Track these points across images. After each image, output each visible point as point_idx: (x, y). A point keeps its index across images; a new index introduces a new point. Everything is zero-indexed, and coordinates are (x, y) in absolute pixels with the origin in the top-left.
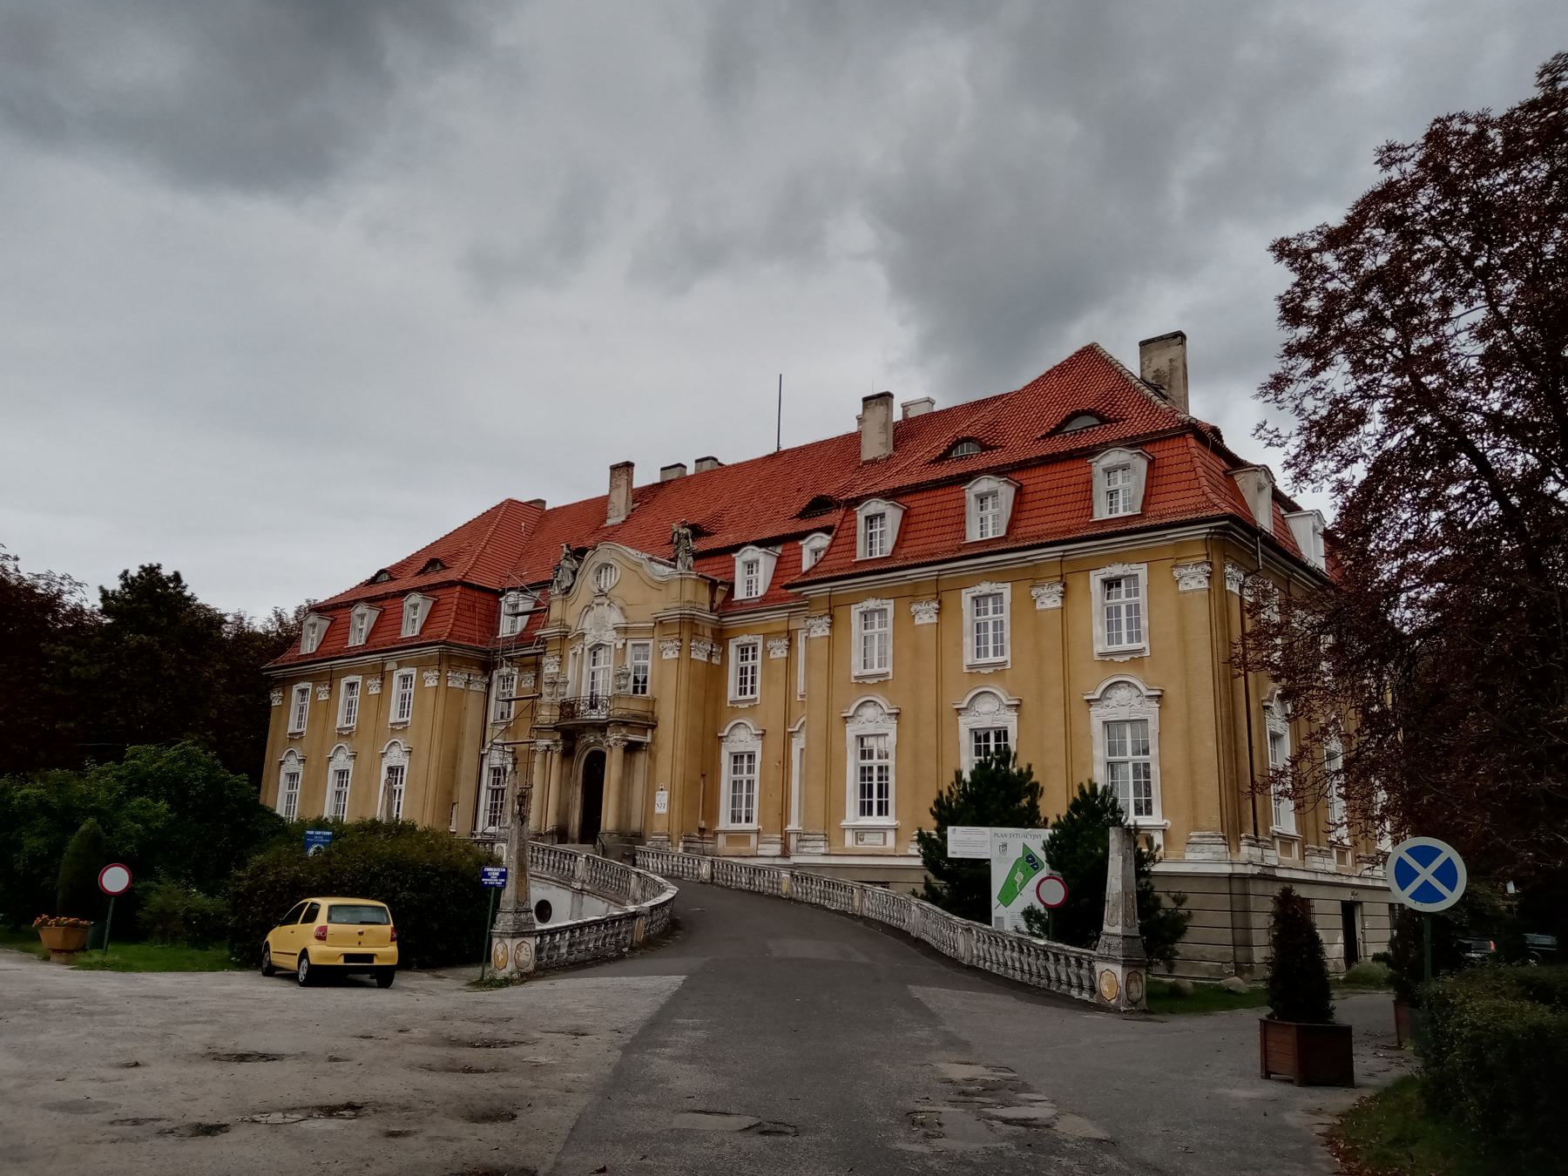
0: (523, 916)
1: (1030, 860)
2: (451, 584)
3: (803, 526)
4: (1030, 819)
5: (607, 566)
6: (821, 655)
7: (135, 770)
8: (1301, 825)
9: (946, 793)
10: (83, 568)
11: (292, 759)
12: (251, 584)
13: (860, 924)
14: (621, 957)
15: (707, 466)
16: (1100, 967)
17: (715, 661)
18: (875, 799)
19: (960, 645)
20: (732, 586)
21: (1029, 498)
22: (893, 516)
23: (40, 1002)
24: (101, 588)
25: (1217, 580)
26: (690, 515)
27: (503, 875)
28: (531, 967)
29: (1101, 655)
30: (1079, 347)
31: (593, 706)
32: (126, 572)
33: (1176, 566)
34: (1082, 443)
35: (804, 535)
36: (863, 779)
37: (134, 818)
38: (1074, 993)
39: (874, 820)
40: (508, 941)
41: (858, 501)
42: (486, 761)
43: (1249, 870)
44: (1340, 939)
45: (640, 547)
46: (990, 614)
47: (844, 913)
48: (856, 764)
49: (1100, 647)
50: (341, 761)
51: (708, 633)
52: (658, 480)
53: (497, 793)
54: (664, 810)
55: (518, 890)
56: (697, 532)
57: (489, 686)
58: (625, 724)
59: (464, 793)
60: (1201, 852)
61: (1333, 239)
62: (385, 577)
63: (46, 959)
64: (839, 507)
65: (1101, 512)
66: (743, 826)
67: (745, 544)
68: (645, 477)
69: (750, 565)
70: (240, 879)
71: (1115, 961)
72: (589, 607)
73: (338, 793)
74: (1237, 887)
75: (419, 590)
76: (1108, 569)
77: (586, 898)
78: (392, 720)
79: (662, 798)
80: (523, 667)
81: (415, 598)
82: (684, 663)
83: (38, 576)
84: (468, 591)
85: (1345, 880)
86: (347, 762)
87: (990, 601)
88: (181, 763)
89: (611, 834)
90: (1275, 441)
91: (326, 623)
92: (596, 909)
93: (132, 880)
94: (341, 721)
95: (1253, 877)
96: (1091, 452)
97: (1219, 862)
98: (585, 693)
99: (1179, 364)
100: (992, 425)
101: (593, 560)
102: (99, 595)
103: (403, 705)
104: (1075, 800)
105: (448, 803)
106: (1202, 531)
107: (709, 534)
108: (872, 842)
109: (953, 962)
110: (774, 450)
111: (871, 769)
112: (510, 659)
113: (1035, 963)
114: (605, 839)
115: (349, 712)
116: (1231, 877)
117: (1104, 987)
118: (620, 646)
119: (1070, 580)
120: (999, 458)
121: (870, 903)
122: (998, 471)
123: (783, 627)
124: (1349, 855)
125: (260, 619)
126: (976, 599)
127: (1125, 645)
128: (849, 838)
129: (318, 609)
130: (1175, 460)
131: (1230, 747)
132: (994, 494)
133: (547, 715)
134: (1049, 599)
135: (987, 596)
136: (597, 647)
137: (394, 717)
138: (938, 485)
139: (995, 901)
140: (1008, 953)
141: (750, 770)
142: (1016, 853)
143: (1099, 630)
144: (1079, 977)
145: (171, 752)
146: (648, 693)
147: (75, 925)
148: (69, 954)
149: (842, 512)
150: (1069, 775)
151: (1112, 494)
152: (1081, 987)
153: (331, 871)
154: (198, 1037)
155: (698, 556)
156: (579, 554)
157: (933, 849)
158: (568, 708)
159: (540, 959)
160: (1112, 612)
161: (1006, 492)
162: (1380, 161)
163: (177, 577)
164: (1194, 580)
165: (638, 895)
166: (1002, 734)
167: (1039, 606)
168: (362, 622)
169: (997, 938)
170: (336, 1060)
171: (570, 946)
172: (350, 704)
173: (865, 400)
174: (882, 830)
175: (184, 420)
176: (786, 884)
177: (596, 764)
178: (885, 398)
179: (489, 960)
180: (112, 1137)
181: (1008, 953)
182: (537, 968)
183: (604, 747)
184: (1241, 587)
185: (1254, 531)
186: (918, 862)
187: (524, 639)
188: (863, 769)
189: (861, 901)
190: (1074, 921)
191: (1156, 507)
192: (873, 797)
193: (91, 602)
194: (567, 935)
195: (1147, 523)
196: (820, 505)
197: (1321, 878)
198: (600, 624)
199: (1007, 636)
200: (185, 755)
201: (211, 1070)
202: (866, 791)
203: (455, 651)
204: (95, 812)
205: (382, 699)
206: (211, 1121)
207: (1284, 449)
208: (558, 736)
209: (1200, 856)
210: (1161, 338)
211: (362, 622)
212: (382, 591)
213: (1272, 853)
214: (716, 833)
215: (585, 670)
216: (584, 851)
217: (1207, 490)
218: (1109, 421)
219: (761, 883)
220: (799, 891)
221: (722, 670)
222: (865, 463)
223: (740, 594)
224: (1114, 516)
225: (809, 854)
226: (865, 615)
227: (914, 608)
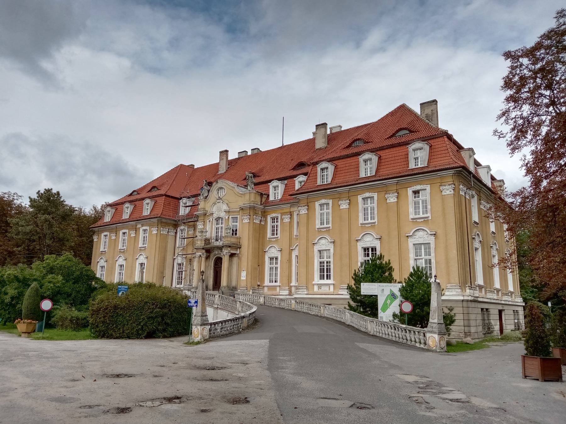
0: (204, 318)
1: (393, 296)
2: (161, 195)
3: (295, 173)
4: (390, 280)
5: (221, 188)
6: (304, 220)
9: (357, 271)
12: (87, 197)
13: (325, 319)
14: (239, 333)
15: (256, 151)
16: (428, 335)
17: (262, 223)
18: (325, 274)
19: (358, 216)
20: (268, 196)
21: (383, 161)
22: (331, 168)
23: (25, 353)
24: (30, 197)
25: (457, 190)
26: (251, 170)
27: (196, 302)
28: (208, 337)
29: (412, 219)
30: (398, 105)
31: (217, 240)
32: (39, 191)
34: (403, 140)
35: (295, 176)
36: (321, 266)
37: (50, 282)
38: (418, 345)
39: (325, 281)
40: (199, 327)
41: (317, 163)
42: (176, 261)
43: (470, 298)
44: (498, 323)
46: (369, 204)
47: (317, 316)
48: (318, 261)
49: (412, 216)
50: (121, 261)
51: (260, 213)
53: (180, 273)
54: (245, 279)
55: (202, 308)
56: (255, 176)
57: (176, 233)
58: (230, 247)
59: (168, 272)
60: (452, 292)
62: (135, 193)
63: (20, 336)
64: (309, 165)
65: (412, 165)
66: (274, 284)
67: (273, 180)
68: (232, 156)
69: (275, 187)
70: (94, 304)
71: (435, 333)
72: (215, 204)
73: (120, 273)
74: (465, 304)
75: (149, 198)
77: (219, 311)
78: (140, 246)
79: (244, 275)
80: (189, 227)
81: (148, 201)
83: (5, 193)
84: (168, 198)
85: (500, 302)
86: (125, 262)
87: (369, 200)
90: (501, 136)
92: (224, 315)
93: (53, 305)
94: (120, 247)
95: (471, 301)
97: (459, 295)
98: (214, 235)
99: (435, 112)
100: (367, 134)
101: (215, 186)
103: (144, 241)
104: (411, 273)
106: (452, 172)
107: (259, 176)
108: (325, 289)
109: (366, 334)
111: (323, 262)
112: (184, 223)
113: (401, 334)
114: (223, 289)
116: (463, 301)
117: (431, 343)
118: (227, 218)
119: (400, 191)
120: (371, 146)
121: (326, 312)
122: (372, 151)
123: (288, 210)
125: (88, 210)
126: (321, 205)
127: (421, 215)
128: (316, 288)
129: (111, 205)
130: (440, 146)
131: (462, 253)
132: (370, 160)
133: (200, 243)
135: (324, 204)
136: (218, 219)
137: (141, 245)
138: (347, 156)
139: (379, 311)
140: (389, 330)
141: (276, 263)
142: (387, 293)
143: (411, 210)
146: (238, 235)
147: (31, 323)
148: (28, 333)
149: (311, 167)
150: (350, 266)
151: (416, 159)
152: (420, 343)
153: (129, 301)
155: (256, 184)
156: (210, 184)
157: (354, 292)
158: (207, 241)
161: (375, 159)
163: (58, 193)
164: (448, 191)
165: (240, 309)
166: (374, 249)
167: (388, 201)
168: (127, 210)
169: (384, 324)
170: (156, 376)
171: (222, 329)
172: (124, 240)
173: (317, 126)
174: (329, 285)
177: (219, 261)
178: (325, 125)
179: (191, 333)
180: (84, 415)
182: (210, 337)
183: (221, 255)
184: (465, 193)
185: (470, 173)
186: (348, 297)
187: (190, 215)
188: (321, 263)
190: (418, 317)
191: (433, 163)
192: (325, 272)
193: (26, 203)
195: (430, 169)
196: (301, 165)
197: (492, 301)
198: (219, 210)
199: (376, 212)
200: (66, 258)
202: (322, 270)
203: (163, 220)
205: (136, 238)
206: (122, 406)
207: (505, 139)
208: (204, 251)
209: (451, 293)
210: (428, 102)
211: (127, 210)
214: (264, 287)
216: (217, 294)
217: (453, 157)
218: (413, 132)
219: (283, 305)
220: (299, 308)
222: (317, 149)
223: (271, 198)
224: (417, 167)
225: (300, 294)
226: (321, 205)
227: (152, 229)
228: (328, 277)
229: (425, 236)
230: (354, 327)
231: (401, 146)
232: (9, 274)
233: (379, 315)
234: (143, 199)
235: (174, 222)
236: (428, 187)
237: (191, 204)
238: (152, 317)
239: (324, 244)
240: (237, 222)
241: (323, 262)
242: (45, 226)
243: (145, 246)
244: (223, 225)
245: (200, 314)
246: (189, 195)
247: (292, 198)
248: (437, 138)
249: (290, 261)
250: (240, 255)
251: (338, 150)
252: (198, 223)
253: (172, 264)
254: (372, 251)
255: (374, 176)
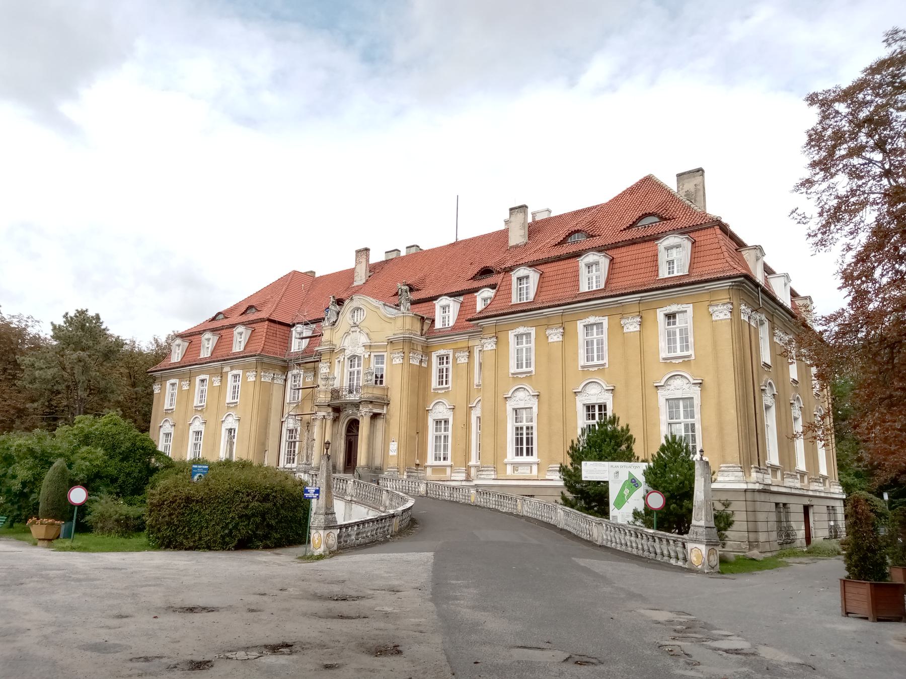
0: (330, 516)
2: (262, 320)
3: (476, 284)
4: (628, 456)
5: (358, 309)
6: (490, 362)
7: (82, 429)
8: (781, 460)
10: (41, 315)
11: (167, 425)
12: (139, 323)
13: (523, 520)
14: (386, 541)
15: (413, 250)
16: (689, 546)
18: (525, 446)
19: (576, 354)
20: (433, 321)
21: (617, 266)
22: (534, 276)
23: (44, 573)
24: (52, 323)
25: (735, 313)
26: (407, 281)
27: (317, 492)
28: (335, 548)
29: (664, 359)
30: (641, 177)
31: (351, 392)
32: (67, 314)
33: (711, 305)
35: (476, 290)
36: (517, 434)
37: (84, 459)
38: (673, 561)
39: (525, 458)
40: (321, 532)
43: (757, 486)
44: (803, 527)
45: (375, 297)
46: (595, 336)
47: (511, 514)
49: (664, 354)
50: (197, 425)
51: (420, 348)
52: (384, 259)
53: (292, 444)
54: (395, 454)
55: (327, 501)
57: (285, 380)
58: (371, 402)
61: (847, 95)
62: (221, 316)
63: (35, 544)
64: (499, 273)
65: (664, 273)
66: (442, 463)
68: (376, 257)
70: (153, 495)
72: (347, 333)
74: (749, 496)
75: (243, 324)
76: (668, 307)
77: (354, 506)
79: (393, 447)
80: (306, 370)
81: (241, 329)
82: (406, 366)
83: (13, 317)
84: (272, 324)
85: (805, 493)
86: (205, 427)
87: (595, 327)
88: (110, 426)
89: (363, 468)
91: (186, 344)
92: (361, 513)
94: (196, 402)
95: (759, 491)
96: (655, 238)
97: (739, 482)
98: (346, 384)
99: (700, 187)
100: (592, 223)
101: (348, 306)
102: (51, 327)
104: (663, 445)
105: (262, 448)
106: (728, 283)
108: (523, 471)
109: (590, 543)
110: (453, 241)
111: (522, 428)
112: (299, 365)
115: (201, 397)
116: (746, 491)
118: (367, 356)
119: (644, 314)
120: (597, 242)
121: (526, 508)
122: (600, 249)
123: (464, 345)
124: (806, 478)
125: (145, 344)
127: (679, 353)
128: (509, 469)
129: (182, 336)
130: (709, 242)
132: (597, 263)
133: (323, 397)
134: (632, 326)
135: (592, 325)
136: (352, 358)
137: (229, 399)
138: (559, 259)
140: (628, 537)
141: (446, 429)
142: (624, 477)
143: (663, 344)
144: (676, 552)
145: (103, 420)
146: (384, 384)
147: (52, 524)
148: (49, 541)
152: (677, 559)
154: (157, 598)
156: (340, 302)
157: (572, 477)
158: (335, 393)
159: (339, 542)
160: (670, 335)
162: (886, 41)
163: (98, 317)
164: (722, 313)
165: (387, 503)
166: (602, 407)
167: (625, 330)
168: (208, 345)
169: (619, 528)
171: (357, 534)
172: (202, 392)
173: (511, 209)
174: (530, 464)
175: (127, 207)
176: (473, 497)
177: (353, 426)
178: (523, 208)
179: (309, 541)
180: (137, 671)
181: (628, 537)
182: (339, 548)
183: (358, 416)
184: (749, 318)
187: (307, 352)
188: (517, 429)
189: (522, 507)
190: (673, 516)
192: (524, 444)
193: (46, 332)
194: (355, 528)
195: (693, 280)
196: (486, 272)
197: (794, 491)
199: (606, 348)
200: (110, 420)
201: (177, 620)
202: (519, 441)
203: (265, 360)
204: (60, 455)
205: (222, 389)
207: (807, 226)
208: (330, 410)
209: (727, 479)
210: (690, 172)
211: (208, 345)
212: (220, 325)
213: (766, 476)
214: (426, 467)
215: (345, 371)
216: (351, 479)
218: (666, 219)
219: (457, 496)
221: (427, 372)
222: (511, 247)
223: (438, 325)
224: (671, 275)
225: (484, 479)
226: (518, 336)
228: (529, 452)
229: (686, 387)
230: (570, 532)
231: (645, 241)
232: (20, 446)
233: (612, 514)
234: (233, 326)
235: (283, 364)
236: (690, 308)
237: (309, 334)
238: (246, 515)
239: (522, 399)
240: (382, 363)
241: (522, 428)
242: (78, 370)
243: (235, 401)
244: (361, 368)
245: (323, 511)
246: (306, 320)
247: (471, 324)
248: (705, 229)
249: (467, 426)
250: (388, 417)
251: (545, 248)
252: (321, 365)
253: (279, 430)
254: (600, 409)
255: (604, 290)
